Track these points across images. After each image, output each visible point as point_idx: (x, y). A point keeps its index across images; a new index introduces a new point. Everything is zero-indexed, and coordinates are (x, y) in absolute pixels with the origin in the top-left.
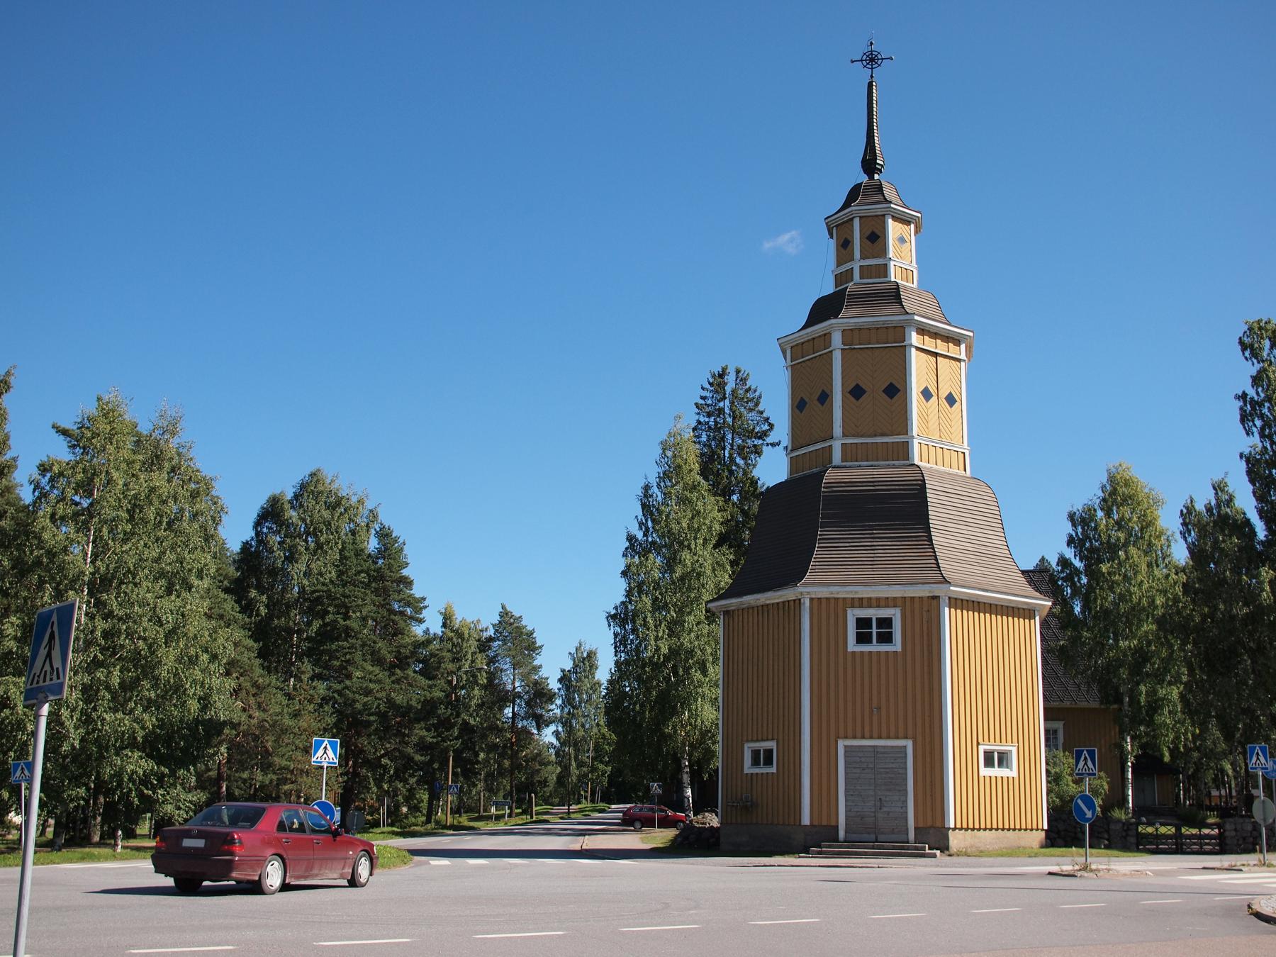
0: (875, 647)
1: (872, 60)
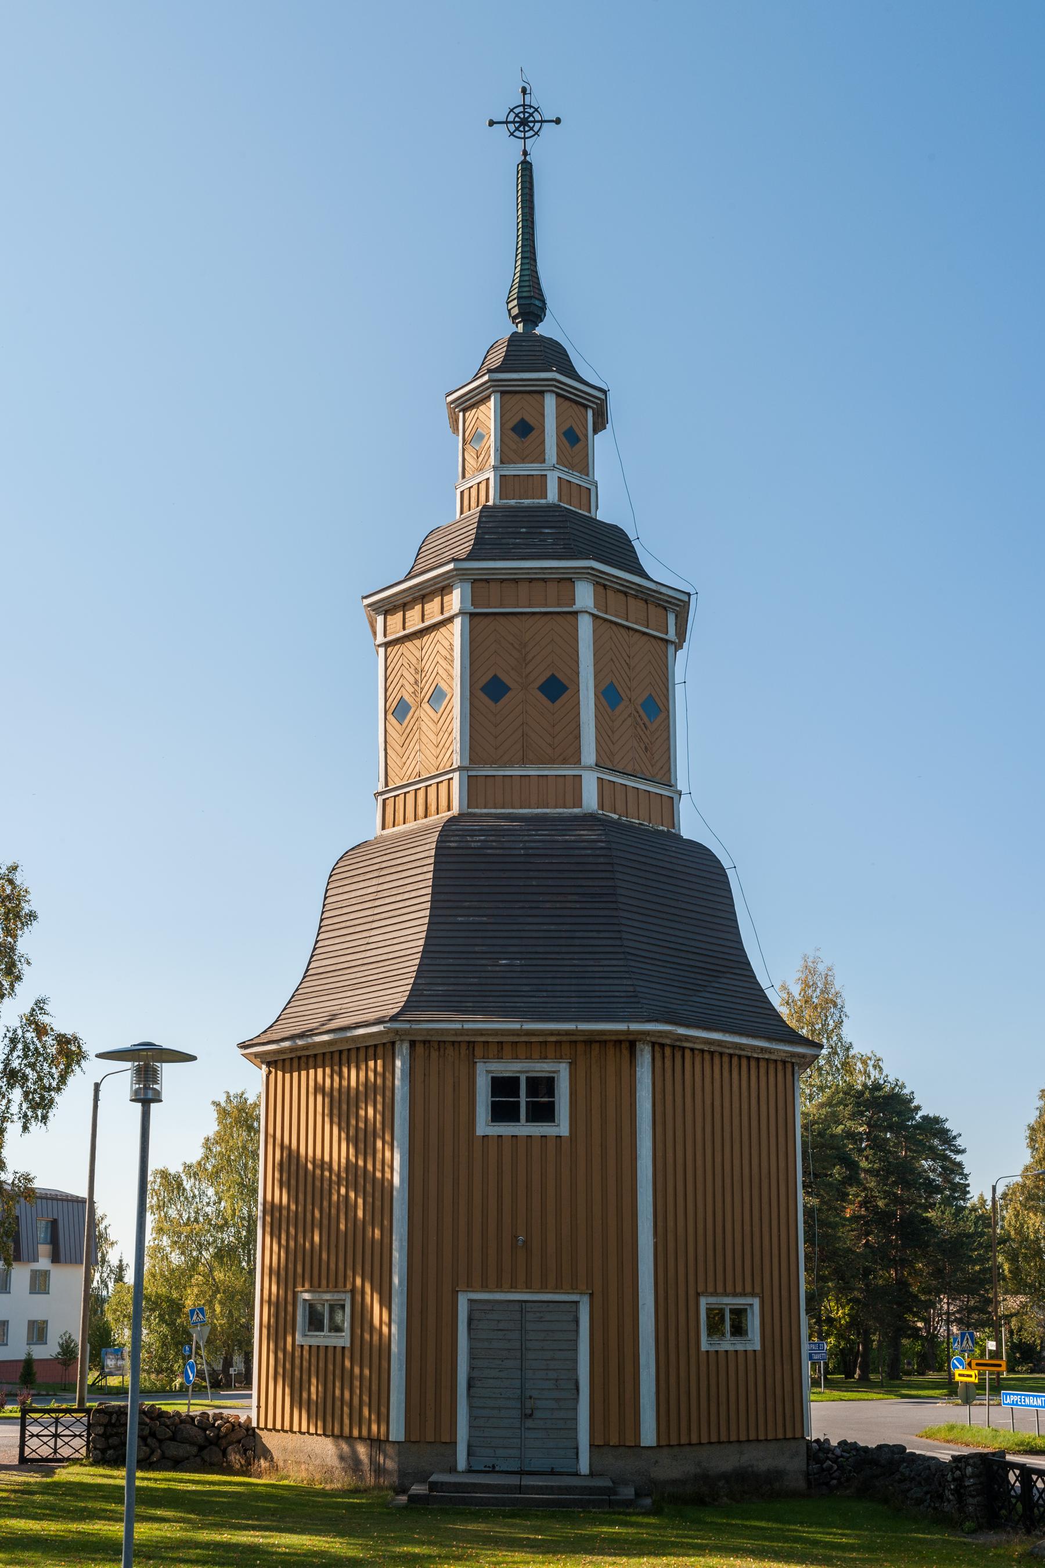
0: (523, 1129)
1: (524, 122)
